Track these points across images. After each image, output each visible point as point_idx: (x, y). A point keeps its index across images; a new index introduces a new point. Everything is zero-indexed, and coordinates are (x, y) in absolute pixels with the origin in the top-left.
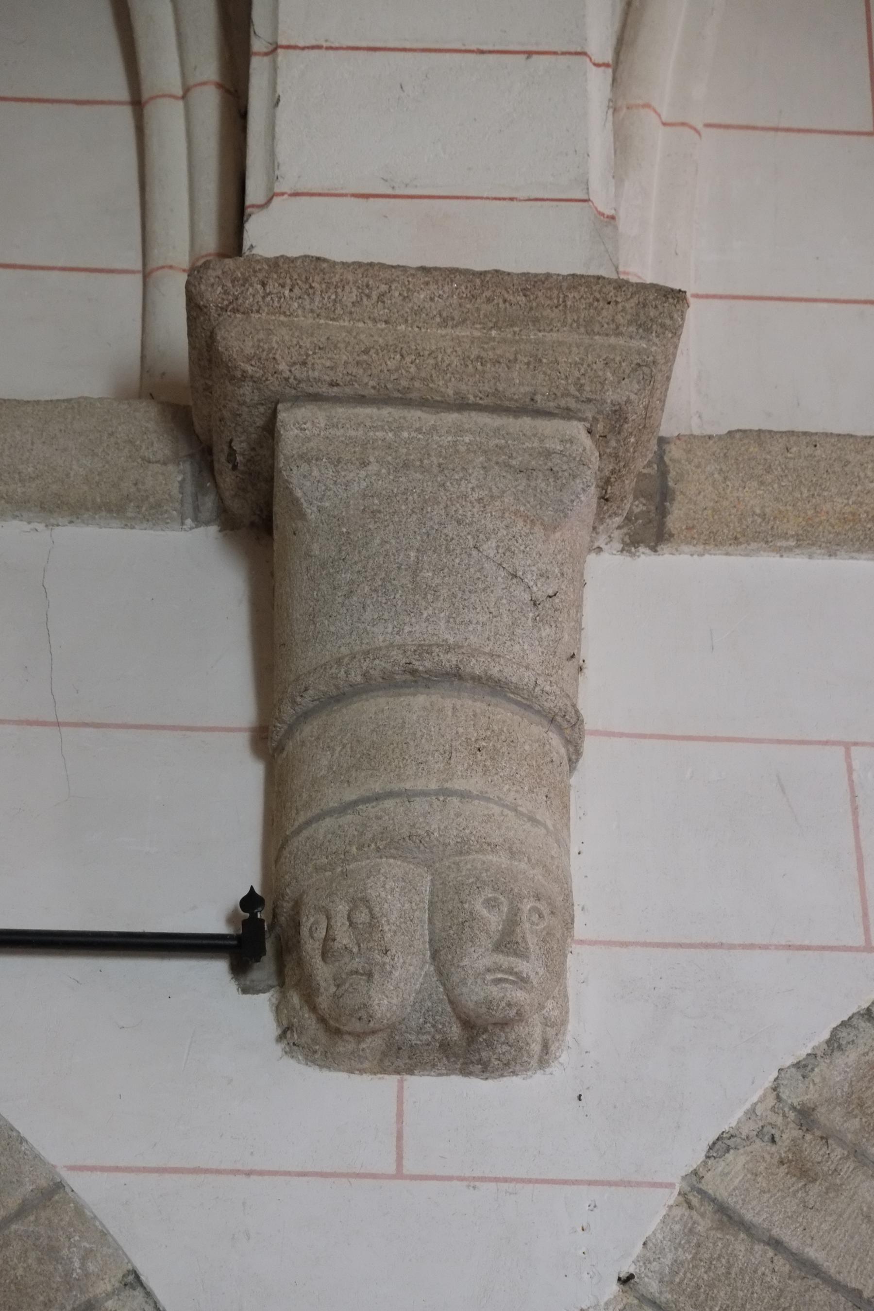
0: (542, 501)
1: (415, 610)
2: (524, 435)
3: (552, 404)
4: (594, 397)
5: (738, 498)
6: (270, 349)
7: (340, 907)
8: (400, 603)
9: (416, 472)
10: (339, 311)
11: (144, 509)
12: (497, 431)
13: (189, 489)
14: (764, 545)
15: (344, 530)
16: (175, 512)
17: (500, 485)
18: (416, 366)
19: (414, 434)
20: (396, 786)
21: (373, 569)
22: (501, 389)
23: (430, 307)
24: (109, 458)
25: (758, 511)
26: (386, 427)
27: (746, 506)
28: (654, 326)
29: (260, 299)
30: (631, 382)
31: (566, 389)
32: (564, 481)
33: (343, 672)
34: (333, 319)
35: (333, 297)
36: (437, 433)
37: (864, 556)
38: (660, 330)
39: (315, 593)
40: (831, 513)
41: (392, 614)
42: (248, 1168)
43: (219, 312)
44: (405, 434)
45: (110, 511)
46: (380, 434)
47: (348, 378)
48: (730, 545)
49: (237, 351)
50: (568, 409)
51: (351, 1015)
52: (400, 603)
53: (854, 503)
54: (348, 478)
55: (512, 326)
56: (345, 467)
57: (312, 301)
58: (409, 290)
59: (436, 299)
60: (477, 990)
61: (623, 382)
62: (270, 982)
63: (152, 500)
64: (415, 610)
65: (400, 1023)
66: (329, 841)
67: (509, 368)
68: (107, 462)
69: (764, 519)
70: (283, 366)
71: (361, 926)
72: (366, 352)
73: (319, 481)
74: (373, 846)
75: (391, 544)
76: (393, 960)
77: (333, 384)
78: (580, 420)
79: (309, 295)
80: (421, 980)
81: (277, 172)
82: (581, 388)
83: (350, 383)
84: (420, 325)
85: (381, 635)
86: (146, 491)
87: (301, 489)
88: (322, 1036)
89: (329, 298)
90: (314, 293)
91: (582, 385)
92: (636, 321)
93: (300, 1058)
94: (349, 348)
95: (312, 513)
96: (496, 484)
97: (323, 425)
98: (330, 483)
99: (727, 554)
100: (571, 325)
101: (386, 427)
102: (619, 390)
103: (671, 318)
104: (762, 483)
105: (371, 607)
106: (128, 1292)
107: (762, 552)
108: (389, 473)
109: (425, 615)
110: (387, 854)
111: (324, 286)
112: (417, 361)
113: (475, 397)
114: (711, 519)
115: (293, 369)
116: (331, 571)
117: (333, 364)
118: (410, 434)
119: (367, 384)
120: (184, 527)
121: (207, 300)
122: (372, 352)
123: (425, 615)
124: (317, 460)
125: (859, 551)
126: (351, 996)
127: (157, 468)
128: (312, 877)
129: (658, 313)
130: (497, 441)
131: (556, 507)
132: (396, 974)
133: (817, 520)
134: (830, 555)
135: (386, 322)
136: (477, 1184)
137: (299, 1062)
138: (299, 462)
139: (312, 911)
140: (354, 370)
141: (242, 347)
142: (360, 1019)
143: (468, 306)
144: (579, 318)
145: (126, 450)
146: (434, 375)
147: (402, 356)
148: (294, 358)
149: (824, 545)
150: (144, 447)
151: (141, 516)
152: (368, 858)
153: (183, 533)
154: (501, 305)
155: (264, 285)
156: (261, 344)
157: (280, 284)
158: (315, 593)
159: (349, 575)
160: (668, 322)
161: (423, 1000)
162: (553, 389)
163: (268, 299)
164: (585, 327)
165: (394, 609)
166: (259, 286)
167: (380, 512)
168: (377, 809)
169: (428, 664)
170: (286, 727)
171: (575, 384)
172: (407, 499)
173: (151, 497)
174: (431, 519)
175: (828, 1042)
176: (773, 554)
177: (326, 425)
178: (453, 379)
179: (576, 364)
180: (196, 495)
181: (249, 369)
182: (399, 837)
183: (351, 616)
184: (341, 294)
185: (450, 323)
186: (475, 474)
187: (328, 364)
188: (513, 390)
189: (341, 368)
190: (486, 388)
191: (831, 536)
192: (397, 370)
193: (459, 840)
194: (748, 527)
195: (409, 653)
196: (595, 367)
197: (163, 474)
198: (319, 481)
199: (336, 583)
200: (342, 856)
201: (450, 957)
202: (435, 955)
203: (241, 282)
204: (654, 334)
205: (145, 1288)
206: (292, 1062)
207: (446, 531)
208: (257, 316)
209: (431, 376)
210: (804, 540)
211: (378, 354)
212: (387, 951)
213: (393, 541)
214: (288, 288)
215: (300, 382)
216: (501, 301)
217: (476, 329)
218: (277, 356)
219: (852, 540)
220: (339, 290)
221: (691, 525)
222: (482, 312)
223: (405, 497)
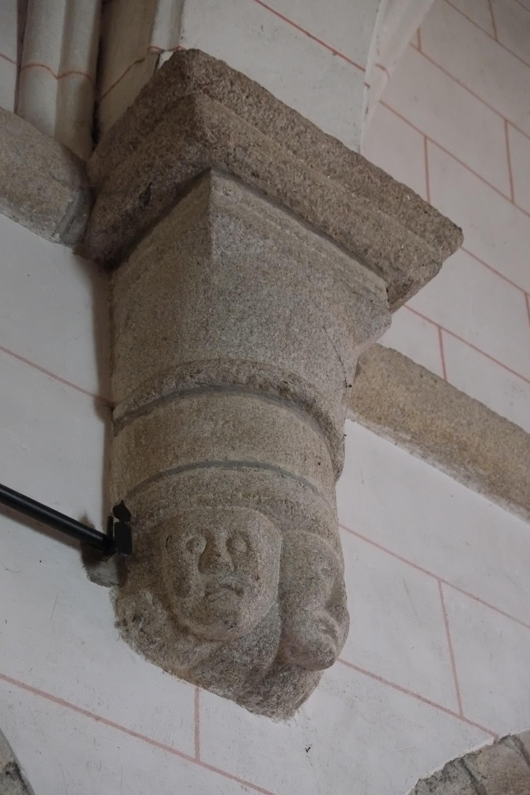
0: (359, 319)
1: (286, 350)
2: (356, 271)
3: (374, 260)
4: (401, 268)
5: (393, 392)
6: (228, 128)
7: (223, 533)
8: (277, 340)
9: (295, 259)
10: (271, 128)
11: (35, 210)
12: (342, 259)
13: (72, 212)
14: (392, 432)
15: (242, 275)
16: (54, 224)
17: (340, 296)
18: (311, 190)
19: (293, 235)
20: (273, 463)
21: (260, 310)
22: (352, 233)
23: (326, 157)
24: (28, 161)
25: (401, 406)
26: (278, 221)
27: (396, 399)
28: (445, 242)
29: (227, 92)
30: (426, 270)
31: (389, 254)
32: (377, 313)
33: (234, 369)
34: (264, 133)
35: (271, 116)
36: (307, 241)
37: (441, 466)
38: (447, 246)
39: (210, 310)
40: (439, 428)
41: (271, 345)
42: (97, 714)
43: (196, 86)
44: (288, 232)
45: (10, 200)
46: (273, 223)
47: (267, 175)
48: (374, 421)
49: (207, 117)
50: (381, 269)
51: (221, 617)
52: (277, 340)
53: (453, 428)
54: (250, 241)
55: (366, 196)
56: (252, 232)
57: (258, 112)
58: (316, 138)
59: (331, 153)
60: (311, 632)
61: (422, 267)
62: (112, 580)
63: (44, 206)
64: (286, 350)
65: (235, 640)
66: (216, 484)
67: (363, 221)
68: (26, 164)
69: (402, 413)
70: (231, 144)
71: (238, 553)
72: (285, 163)
73: (231, 234)
74: (257, 498)
75: (274, 298)
76: (260, 586)
77: (255, 174)
78: (386, 280)
79: (257, 106)
80: (268, 611)
81: (182, 34)
82: (397, 258)
83: (265, 179)
84: (313, 166)
85: (262, 356)
86: (44, 198)
87: (216, 233)
88: (169, 632)
89: (269, 116)
90: (261, 107)
91: (399, 256)
92: (437, 233)
93: (134, 644)
94: (275, 155)
95: (215, 257)
96: (337, 294)
97: (240, 198)
98: (237, 238)
99: (368, 428)
100: (400, 215)
101: (278, 221)
102: (417, 271)
103: (456, 242)
104: (408, 389)
105: (257, 334)
106: (7, 780)
107: (387, 436)
108: (278, 251)
109: (292, 356)
110: (263, 509)
111: (268, 106)
112: (312, 187)
113: (334, 230)
114: (374, 398)
115: (237, 149)
116: (228, 298)
117: (263, 160)
118: (291, 233)
119: (276, 185)
120: (53, 238)
121: (193, 74)
122: (288, 165)
123: (292, 356)
124: (237, 218)
125: (440, 461)
126: (223, 602)
127: (58, 185)
128: (192, 506)
129: (449, 234)
130: (340, 267)
131: (366, 328)
132: (260, 598)
133: (430, 428)
134: (423, 457)
135: (295, 152)
136: (248, 787)
137: (131, 646)
138: (224, 214)
139: (194, 531)
140: (273, 170)
141: (211, 115)
142: (226, 623)
143: (347, 168)
144: (407, 212)
145: (40, 162)
146: (319, 202)
147: (305, 178)
148: (240, 142)
149: (424, 448)
150: (52, 167)
151: (29, 214)
152: (247, 506)
153: (49, 242)
154: (366, 179)
155: (232, 84)
156: (223, 121)
157: (241, 89)
158: (210, 310)
159: (242, 306)
160: (453, 243)
161: (265, 627)
162: (382, 250)
163: (231, 95)
164: (407, 220)
165: (272, 343)
166: (229, 83)
167: (268, 273)
168: (259, 473)
169: (297, 389)
170: (158, 396)
171: (395, 254)
172: (287, 274)
173: (45, 204)
174: (301, 295)
175: (443, 772)
176: (392, 440)
177: (242, 199)
178: (328, 211)
179: (400, 240)
180: (73, 219)
181: (209, 134)
182: (278, 498)
183: (241, 335)
184: (277, 117)
185: (332, 174)
186: (329, 280)
187: (260, 158)
188: (359, 237)
189: (266, 165)
190: (344, 228)
191: (433, 443)
192: (299, 185)
193: (314, 518)
194: (391, 413)
195: (285, 376)
196: (410, 248)
197: (60, 192)
198: (231, 234)
199: (231, 308)
200: (229, 497)
201: (298, 600)
202: (283, 596)
203: (218, 74)
204: (441, 247)
205: (23, 781)
206: (127, 646)
207: (309, 307)
208: (219, 103)
209: (317, 201)
210: (416, 439)
211: (291, 169)
212: (258, 578)
213: (276, 298)
214: (246, 94)
215: (236, 161)
216: (367, 176)
217: (345, 187)
218: (231, 135)
219: (441, 452)
220: (276, 114)
221: (361, 396)
222: (354, 177)
223: (286, 272)
